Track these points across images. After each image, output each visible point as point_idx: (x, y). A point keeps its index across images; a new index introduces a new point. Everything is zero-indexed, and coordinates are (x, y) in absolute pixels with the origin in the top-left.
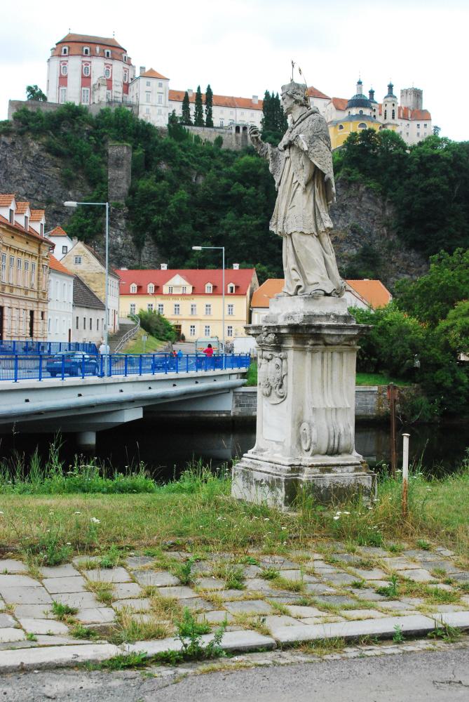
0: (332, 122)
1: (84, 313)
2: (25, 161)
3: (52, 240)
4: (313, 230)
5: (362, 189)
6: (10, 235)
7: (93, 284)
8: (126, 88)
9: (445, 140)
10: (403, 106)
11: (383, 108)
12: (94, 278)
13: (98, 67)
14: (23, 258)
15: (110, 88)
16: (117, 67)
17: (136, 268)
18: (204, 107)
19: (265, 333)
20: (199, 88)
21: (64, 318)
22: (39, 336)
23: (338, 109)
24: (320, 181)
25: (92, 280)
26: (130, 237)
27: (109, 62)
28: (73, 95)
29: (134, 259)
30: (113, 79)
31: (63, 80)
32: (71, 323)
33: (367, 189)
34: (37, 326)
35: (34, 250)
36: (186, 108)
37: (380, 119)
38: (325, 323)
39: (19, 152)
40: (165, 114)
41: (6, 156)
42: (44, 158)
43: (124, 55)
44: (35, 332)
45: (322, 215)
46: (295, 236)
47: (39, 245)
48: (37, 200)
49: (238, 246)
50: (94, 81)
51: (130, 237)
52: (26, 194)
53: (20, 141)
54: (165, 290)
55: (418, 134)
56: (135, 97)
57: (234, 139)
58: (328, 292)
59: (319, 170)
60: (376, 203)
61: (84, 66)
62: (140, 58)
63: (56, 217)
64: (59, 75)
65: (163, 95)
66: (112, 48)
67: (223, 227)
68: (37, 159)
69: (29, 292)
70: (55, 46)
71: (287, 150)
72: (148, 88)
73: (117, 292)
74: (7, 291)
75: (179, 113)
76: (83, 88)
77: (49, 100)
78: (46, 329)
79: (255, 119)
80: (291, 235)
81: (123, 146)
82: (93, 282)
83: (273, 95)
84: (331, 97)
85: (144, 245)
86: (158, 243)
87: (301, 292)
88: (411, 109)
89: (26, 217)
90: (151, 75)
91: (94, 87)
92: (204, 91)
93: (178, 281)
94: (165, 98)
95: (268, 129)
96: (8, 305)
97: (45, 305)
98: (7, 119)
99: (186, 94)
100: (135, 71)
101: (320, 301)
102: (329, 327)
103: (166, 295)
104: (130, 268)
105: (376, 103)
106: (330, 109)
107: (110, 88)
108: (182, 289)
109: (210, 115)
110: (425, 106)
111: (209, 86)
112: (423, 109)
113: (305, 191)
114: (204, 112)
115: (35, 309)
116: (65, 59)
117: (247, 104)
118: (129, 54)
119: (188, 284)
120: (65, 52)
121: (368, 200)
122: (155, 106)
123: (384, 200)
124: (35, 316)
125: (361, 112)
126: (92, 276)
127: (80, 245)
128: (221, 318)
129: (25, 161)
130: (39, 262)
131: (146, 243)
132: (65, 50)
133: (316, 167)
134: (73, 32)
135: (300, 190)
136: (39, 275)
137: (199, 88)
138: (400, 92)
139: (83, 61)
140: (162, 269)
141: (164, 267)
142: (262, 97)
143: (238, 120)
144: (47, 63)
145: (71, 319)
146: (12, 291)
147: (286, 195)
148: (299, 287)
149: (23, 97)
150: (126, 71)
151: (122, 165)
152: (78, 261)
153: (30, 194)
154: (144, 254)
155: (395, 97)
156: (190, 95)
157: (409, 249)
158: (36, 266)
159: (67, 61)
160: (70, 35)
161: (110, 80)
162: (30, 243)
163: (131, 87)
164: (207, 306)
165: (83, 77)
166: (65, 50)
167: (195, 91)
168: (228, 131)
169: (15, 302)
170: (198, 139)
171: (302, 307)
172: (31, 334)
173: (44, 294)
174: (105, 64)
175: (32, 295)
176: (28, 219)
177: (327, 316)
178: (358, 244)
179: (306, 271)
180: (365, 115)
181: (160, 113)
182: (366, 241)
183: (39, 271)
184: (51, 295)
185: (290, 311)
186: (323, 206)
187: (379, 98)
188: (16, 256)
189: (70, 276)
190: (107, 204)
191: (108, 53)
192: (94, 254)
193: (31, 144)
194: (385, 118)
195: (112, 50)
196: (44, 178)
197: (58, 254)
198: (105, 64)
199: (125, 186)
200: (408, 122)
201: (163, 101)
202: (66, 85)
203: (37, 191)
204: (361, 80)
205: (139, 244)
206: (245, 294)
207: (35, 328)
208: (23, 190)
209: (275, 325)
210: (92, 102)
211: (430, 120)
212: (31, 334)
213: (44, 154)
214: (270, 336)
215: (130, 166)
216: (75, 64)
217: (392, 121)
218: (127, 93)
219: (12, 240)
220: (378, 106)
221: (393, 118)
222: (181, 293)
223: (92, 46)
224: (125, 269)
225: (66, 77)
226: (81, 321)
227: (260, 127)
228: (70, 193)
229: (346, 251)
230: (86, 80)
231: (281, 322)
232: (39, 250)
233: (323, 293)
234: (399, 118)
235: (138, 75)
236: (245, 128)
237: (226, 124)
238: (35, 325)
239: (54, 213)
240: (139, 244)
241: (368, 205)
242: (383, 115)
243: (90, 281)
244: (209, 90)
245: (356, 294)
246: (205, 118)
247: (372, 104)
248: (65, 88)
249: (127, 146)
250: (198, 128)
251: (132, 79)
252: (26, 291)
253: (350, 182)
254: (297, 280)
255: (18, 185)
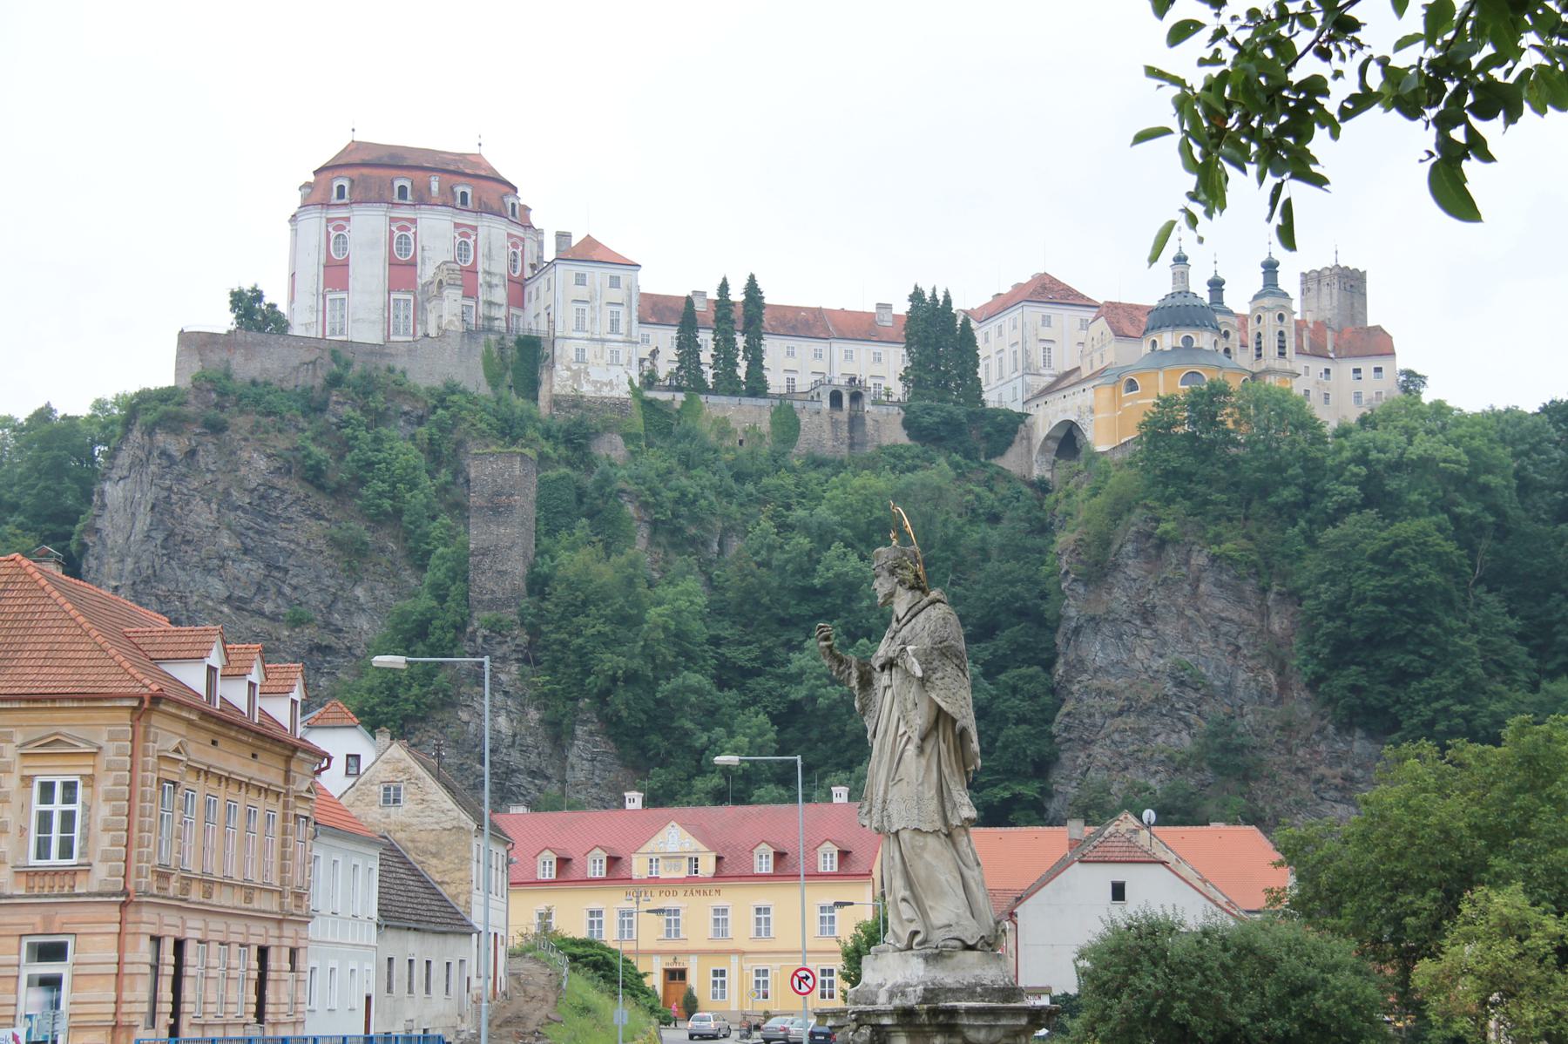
0: (1104, 370)
1: (412, 946)
2: (225, 500)
3: (319, 740)
4: (939, 825)
5: (1199, 560)
6: (206, 738)
7: (434, 861)
8: (518, 290)
9: (1439, 408)
10: (1310, 318)
11: (1252, 326)
12: (438, 842)
13: (436, 233)
14: (242, 799)
15: (471, 293)
16: (493, 232)
17: (554, 806)
18: (741, 341)
19: (854, 1025)
20: (724, 288)
21: (353, 965)
22: (283, 1018)
23: (1120, 334)
24: (949, 732)
25: (433, 849)
26: (534, 715)
27: (468, 219)
28: (364, 317)
29: (547, 778)
30: (480, 268)
31: (336, 273)
32: (373, 974)
33: (1214, 559)
34: (277, 992)
35: (273, 777)
36: (688, 347)
37: (1245, 359)
38: (963, 1004)
39: (209, 477)
40: (630, 363)
41: (170, 489)
42: (284, 492)
43: (510, 200)
44: (269, 1008)
45: (955, 793)
46: (904, 835)
47: (288, 760)
48: (262, 614)
49: (843, 734)
50: (426, 273)
51: (534, 715)
52: (229, 597)
53: (210, 447)
54: (639, 867)
55: (1358, 396)
56: (543, 317)
57: (827, 427)
58: (970, 943)
59: (946, 714)
60: (1241, 600)
61: (397, 234)
62: (553, 210)
63: (322, 661)
64: (323, 261)
65: (622, 310)
66: (475, 182)
67: (797, 678)
68: (262, 497)
69: (256, 894)
70: (311, 178)
71: (887, 672)
72: (582, 293)
73: (499, 879)
74: (196, 894)
75: (666, 365)
76: (393, 296)
77: (297, 330)
78: (302, 996)
79: (885, 368)
80: (897, 833)
81: (512, 455)
82: (434, 855)
83: (934, 295)
84: (1101, 301)
85: (573, 736)
86: (613, 727)
87: (919, 944)
88: (1336, 327)
89: (252, 685)
90: (585, 253)
91: (423, 292)
92: (737, 295)
93: (674, 840)
94: (628, 318)
95: (923, 397)
96: (199, 935)
97: (301, 928)
98: (172, 384)
99: (689, 301)
100: (541, 245)
101: (955, 960)
102: (970, 1012)
103: (641, 881)
104: (534, 806)
105: (1230, 313)
106: (1097, 336)
107: (471, 293)
108: (685, 863)
109: (756, 361)
110: (1376, 314)
111: (752, 278)
112: (1370, 323)
113: (921, 750)
114: (741, 353)
115: (272, 942)
116: (342, 213)
117: (860, 328)
118: (525, 197)
119: (702, 848)
120: (341, 194)
121: (1216, 591)
122: (603, 341)
123: (1264, 590)
124: (272, 964)
125: (1188, 340)
126: (432, 837)
127: (398, 751)
128: (799, 946)
129: (225, 500)
130: (286, 806)
131: (579, 730)
132: (341, 188)
133: (939, 709)
134: (363, 136)
135: (911, 749)
136: (284, 844)
137: (724, 288)
138: (1298, 279)
139: (393, 220)
140: (629, 806)
141: (634, 800)
142: (902, 307)
143: (837, 373)
144: (288, 226)
145: (370, 966)
146: (208, 894)
147: (886, 758)
148: (916, 933)
149: (223, 321)
150: (515, 245)
151: (510, 508)
152: (392, 797)
153: (240, 599)
154: (572, 759)
155: (1286, 295)
156: (699, 306)
157: (1345, 727)
158: (278, 816)
159: (348, 219)
160: (356, 146)
161: (473, 271)
162: (261, 755)
163: (531, 289)
164: (758, 910)
165: (393, 263)
166: (341, 188)
167: (713, 295)
168: (808, 405)
169: (216, 924)
170: (724, 430)
171: (921, 973)
172: (260, 1014)
173: (299, 896)
174: (457, 226)
175: (263, 903)
176: (258, 689)
177: (969, 991)
178: (1193, 718)
179: (928, 903)
180: (1200, 349)
181: (615, 360)
182: (1216, 709)
183: (284, 832)
184: (318, 900)
185: (900, 980)
186: (957, 778)
187: (1238, 299)
188: (222, 793)
189: (370, 842)
190: (486, 659)
191: (464, 195)
192: (438, 777)
193: (245, 455)
194: (1259, 356)
195: (474, 187)
196: (282, 550)
197: (334, 780)
198: (457, 226)
199: (517, 569)
200: (1325, 364)
201: (623, 328)
202: (345, 288)
203: (260, 589)
204: (1186, 252)
205: (558, 733)
206: (870, 874)
207: (270, 995)
208: (219, 585)
209: (869, 1008)
210: (420, 334)
211: (1393, 354)
212: (260, 1014)
213: (279, 482)
214: (863, 1030)
215: (532, 512)
216: (368, 226)
217: (1278, 364)
218: (521, 306)
219: (213, 750)
220: (1236, 322)
221: (1282, 354)
222: (684, 873)
223: (419, 175)
224: (522, 810)
225: (345, 264)
226: (400, 968)
227: (899, 391)
228: (359, 592)
229: (1160, 740)
230: (401, 270)
231: (882, 1002)
232: (287, 772)
233: (958, 943)
234: (1300, 351)
235: (549, 254)
236: (856, 397)
237: (803, 383)
238: (270, 987)
239: (311, 650)
240: (558, 733)
241: (1218, 605)
242: (1252, 346)
243: (424, 852)
244: (752, 288)
245: (1185, 870)
246: (741, 372)
247: (1219, 318)
248: (344, 295)
249: (523, 455)
250: (724, 400)
251: (533, 267)
252: (249, 890)
253: (1162, 543)
254: (911, 921)
255: (208, 571)
